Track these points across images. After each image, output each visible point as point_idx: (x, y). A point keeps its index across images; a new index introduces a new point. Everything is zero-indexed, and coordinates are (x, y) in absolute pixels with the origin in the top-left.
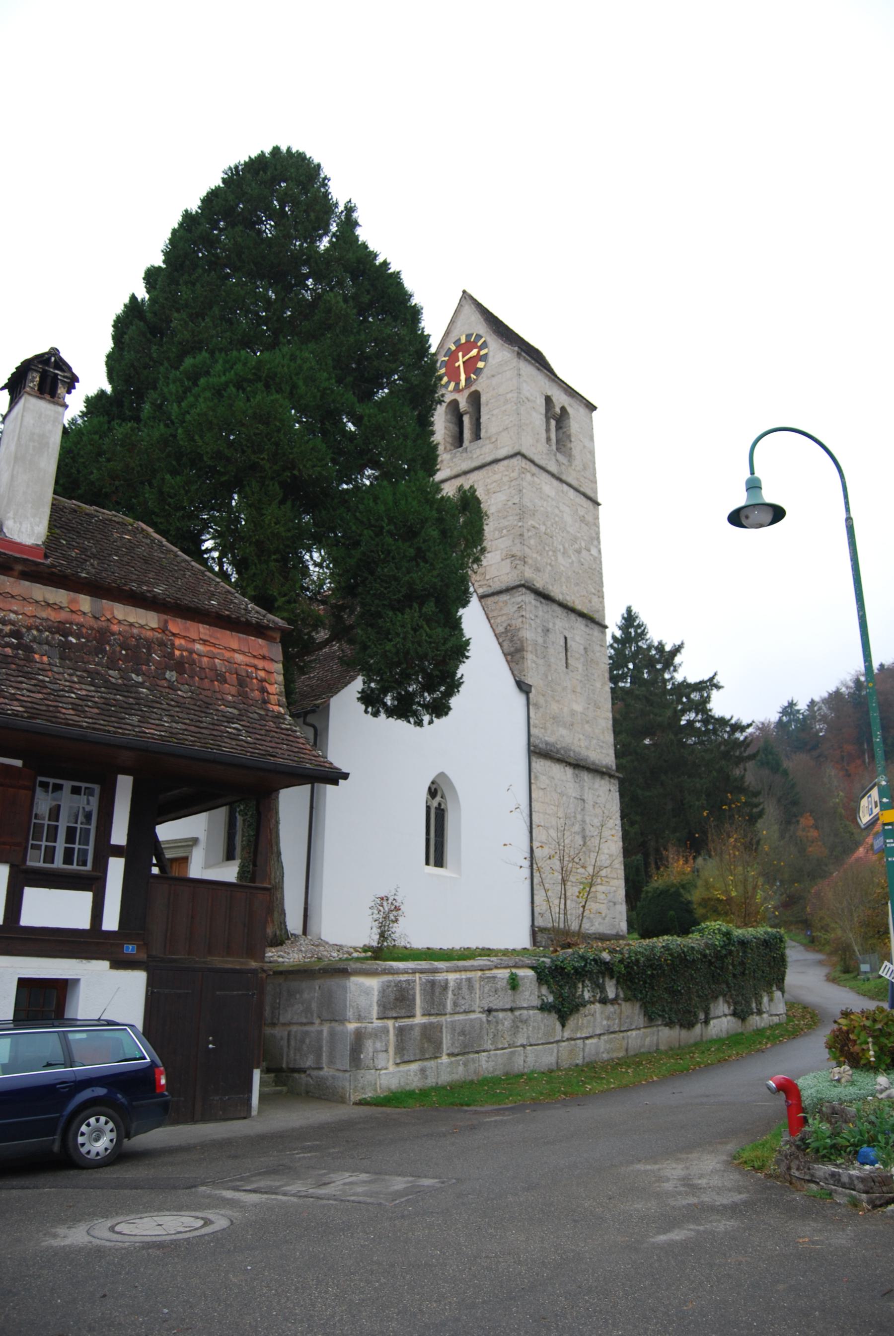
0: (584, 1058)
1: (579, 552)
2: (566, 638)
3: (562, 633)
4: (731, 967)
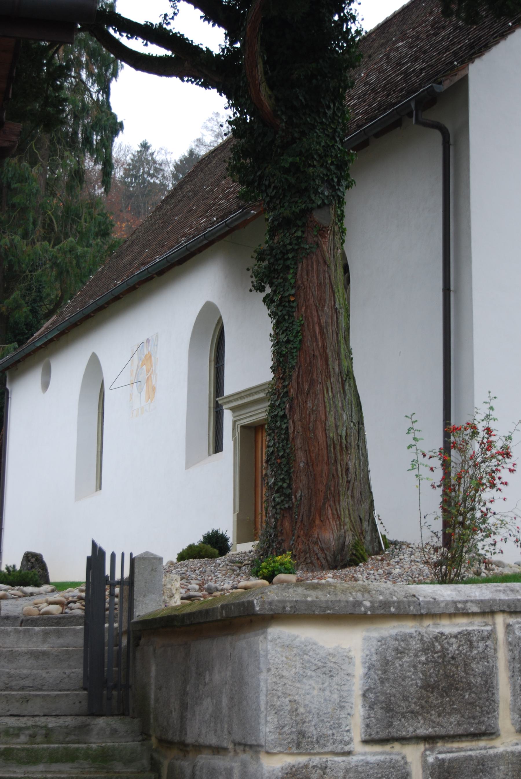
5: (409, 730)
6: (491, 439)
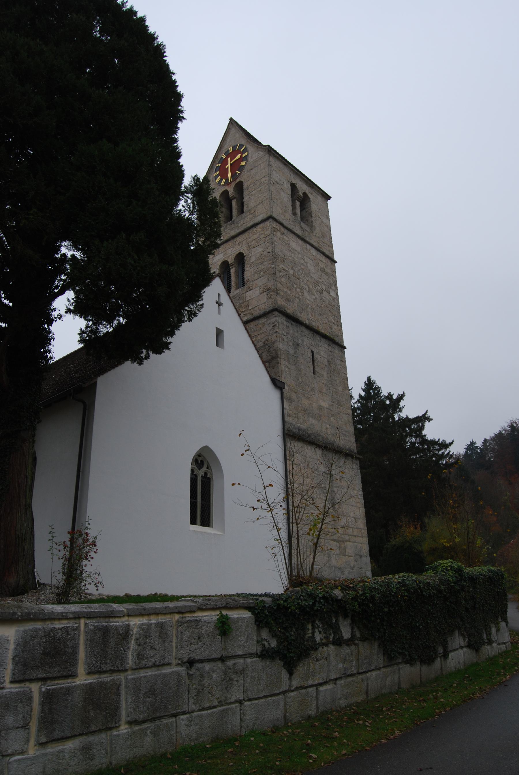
0: (318, 708)
1: (321, 292)
2: (313, 352)
3: (309, 348)
4: (463, 602)
5: (34, 675)
6: (88, 537)
